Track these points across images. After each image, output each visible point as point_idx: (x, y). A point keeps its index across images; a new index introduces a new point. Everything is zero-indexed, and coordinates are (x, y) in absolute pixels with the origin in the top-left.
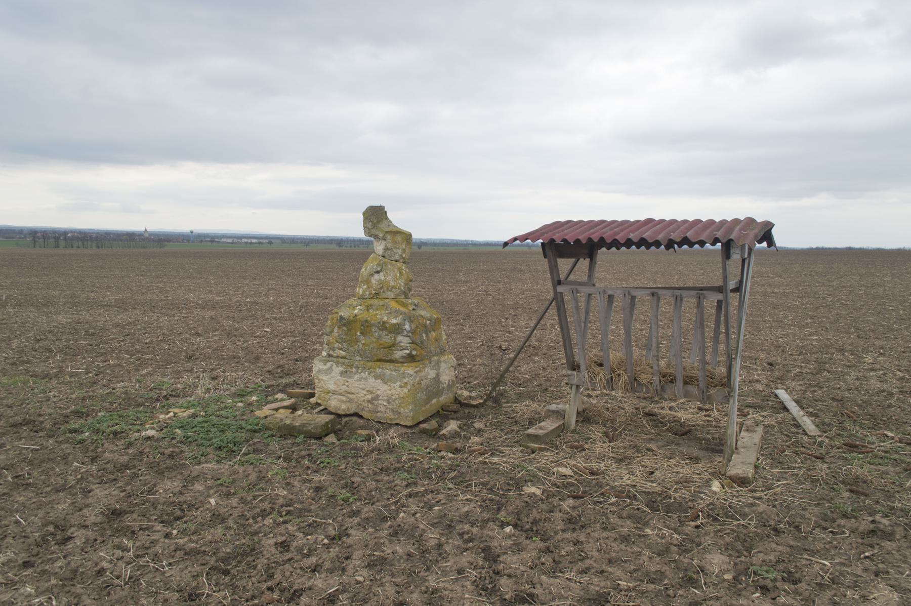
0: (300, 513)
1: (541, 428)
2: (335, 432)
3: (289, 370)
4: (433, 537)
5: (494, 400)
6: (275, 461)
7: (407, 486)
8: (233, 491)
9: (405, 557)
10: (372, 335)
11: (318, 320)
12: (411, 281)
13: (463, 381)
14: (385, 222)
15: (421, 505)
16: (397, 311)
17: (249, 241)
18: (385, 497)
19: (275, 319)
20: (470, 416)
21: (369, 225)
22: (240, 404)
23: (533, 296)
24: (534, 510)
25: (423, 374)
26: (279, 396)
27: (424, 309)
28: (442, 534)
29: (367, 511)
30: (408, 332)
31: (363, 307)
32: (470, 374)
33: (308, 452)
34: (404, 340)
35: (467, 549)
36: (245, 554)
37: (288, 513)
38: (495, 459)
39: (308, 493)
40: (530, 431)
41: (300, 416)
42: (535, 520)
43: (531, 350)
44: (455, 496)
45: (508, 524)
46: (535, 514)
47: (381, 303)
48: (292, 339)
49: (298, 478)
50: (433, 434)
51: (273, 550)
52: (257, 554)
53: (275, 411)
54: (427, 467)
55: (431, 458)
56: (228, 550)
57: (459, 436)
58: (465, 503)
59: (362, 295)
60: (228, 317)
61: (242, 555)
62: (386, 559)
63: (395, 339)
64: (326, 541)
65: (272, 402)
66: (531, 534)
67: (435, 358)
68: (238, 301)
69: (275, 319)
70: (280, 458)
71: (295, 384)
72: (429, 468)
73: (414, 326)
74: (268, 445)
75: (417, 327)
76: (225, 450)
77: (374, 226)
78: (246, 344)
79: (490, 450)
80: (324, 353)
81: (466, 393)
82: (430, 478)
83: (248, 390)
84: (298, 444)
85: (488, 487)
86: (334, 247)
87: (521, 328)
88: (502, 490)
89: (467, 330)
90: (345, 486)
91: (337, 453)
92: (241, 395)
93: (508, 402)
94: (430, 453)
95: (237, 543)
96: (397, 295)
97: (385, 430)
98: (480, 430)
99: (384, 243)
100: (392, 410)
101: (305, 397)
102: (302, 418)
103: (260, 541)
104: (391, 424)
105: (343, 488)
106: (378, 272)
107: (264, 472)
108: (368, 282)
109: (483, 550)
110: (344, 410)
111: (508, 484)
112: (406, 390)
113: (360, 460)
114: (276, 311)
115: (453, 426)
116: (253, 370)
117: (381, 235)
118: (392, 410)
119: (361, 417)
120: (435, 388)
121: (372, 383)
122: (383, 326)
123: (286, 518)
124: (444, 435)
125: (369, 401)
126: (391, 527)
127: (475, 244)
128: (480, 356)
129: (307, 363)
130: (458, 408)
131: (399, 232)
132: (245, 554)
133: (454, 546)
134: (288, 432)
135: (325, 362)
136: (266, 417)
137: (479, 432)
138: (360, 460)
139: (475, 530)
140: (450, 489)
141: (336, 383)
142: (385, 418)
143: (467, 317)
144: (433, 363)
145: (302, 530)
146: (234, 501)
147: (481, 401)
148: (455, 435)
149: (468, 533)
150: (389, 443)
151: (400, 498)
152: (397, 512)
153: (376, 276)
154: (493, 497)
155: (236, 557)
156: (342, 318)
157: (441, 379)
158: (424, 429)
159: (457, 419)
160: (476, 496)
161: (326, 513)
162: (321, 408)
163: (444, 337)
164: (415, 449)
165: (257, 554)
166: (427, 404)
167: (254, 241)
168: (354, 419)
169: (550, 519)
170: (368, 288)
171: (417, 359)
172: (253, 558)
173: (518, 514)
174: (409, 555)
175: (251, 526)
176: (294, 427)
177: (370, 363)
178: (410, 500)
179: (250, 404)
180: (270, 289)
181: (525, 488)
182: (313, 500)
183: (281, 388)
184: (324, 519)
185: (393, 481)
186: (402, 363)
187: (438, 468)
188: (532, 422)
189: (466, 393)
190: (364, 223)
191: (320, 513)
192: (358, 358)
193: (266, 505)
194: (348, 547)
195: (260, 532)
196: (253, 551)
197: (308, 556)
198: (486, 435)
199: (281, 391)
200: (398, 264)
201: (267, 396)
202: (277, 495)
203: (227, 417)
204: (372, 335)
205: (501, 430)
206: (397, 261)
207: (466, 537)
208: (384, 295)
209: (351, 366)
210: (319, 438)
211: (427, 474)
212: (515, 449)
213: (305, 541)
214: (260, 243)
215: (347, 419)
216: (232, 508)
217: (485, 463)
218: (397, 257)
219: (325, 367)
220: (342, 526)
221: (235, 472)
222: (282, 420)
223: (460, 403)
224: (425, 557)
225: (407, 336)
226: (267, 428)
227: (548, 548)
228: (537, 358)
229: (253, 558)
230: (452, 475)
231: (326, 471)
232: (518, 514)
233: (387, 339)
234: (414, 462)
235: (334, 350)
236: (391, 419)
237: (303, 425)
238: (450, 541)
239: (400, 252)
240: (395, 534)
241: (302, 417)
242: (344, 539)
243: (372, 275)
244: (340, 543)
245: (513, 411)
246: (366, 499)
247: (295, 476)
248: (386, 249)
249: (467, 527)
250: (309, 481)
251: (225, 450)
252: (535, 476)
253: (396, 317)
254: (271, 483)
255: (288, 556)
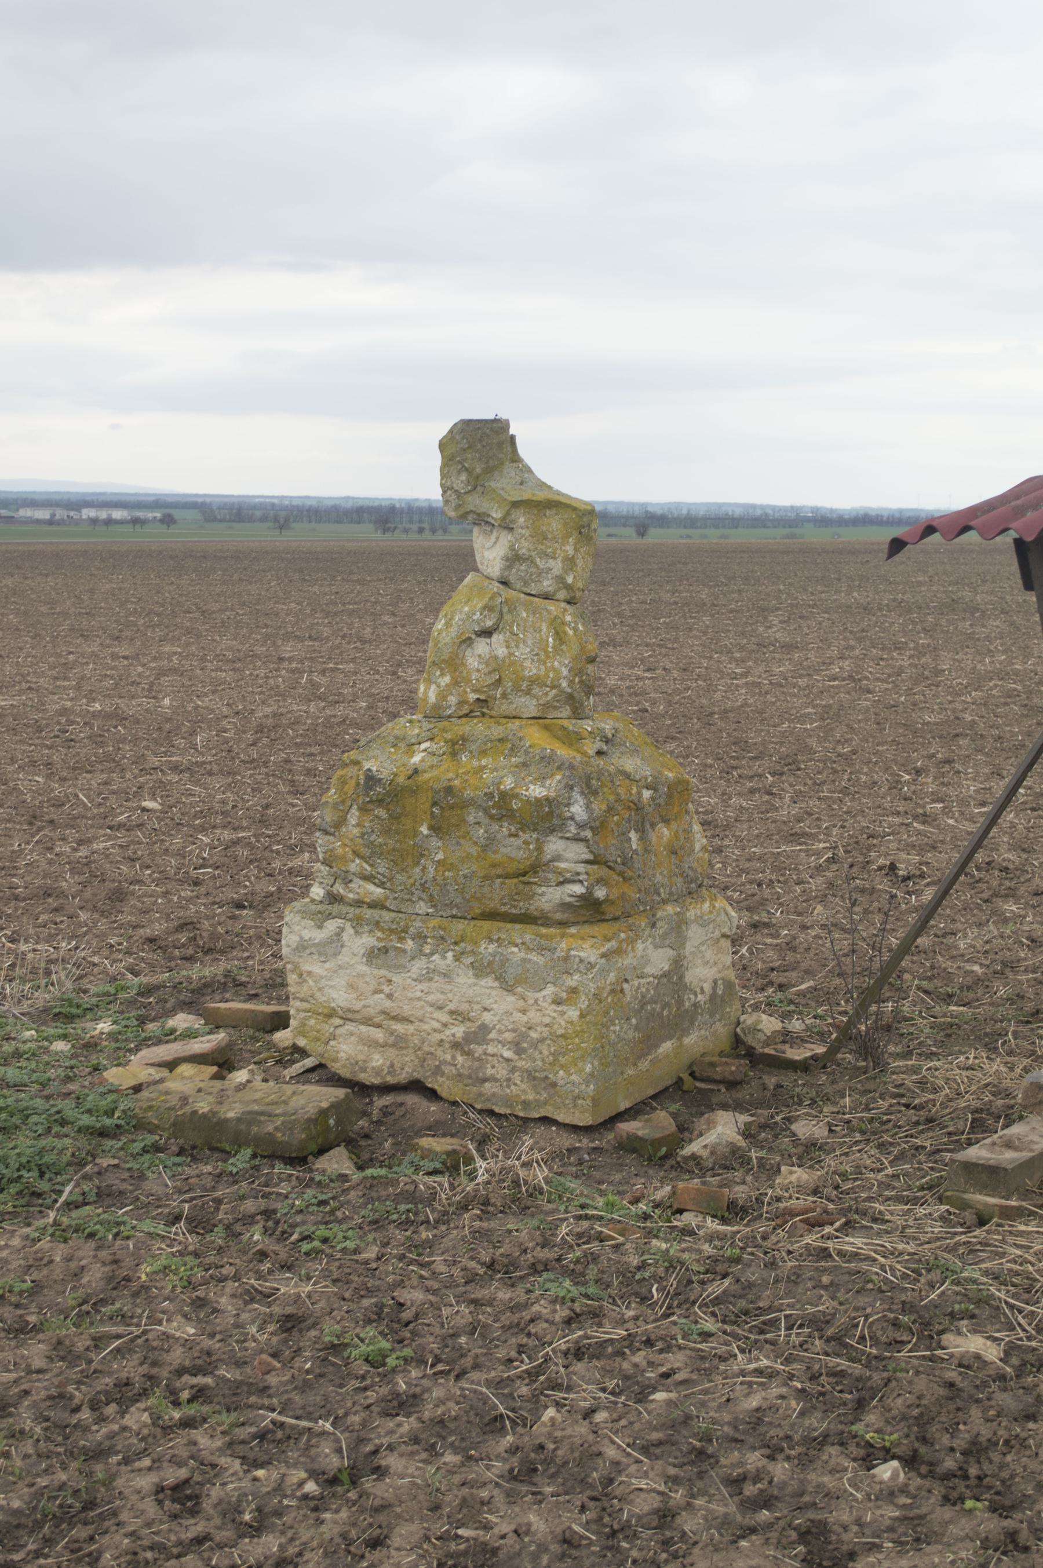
0: (236, 1397)
1: (1009, 1145)
2: (351, 1143)
3: (214, 936)
4: (644, 1487)
5: (862, 1046)
6: (161, 1229)
7: (568, 1322)
8: (32, 1319)
9: (555, 1548)
10: (466, 835)
11: (310, 772)
12: (592, 660)
13: (767, 981)
14: (509, 470)
15: (611, 1384)
16: (548, 759)
17: (103, 515)
18: (501, 1354)
19: (176, 768)
20: (779, 1098)
21: (460, 481)
22: (60, 1046)
23: (1010, 694)
24: (975, 1412)
25: (628, 961)
26: (181, 1021)
27: (635, 752)
28: (675, 1480)
29: (441, 1397)
30: (581, 826)
31: (439, 746)
32: (790, 957)
33: (263, 1204)
34: (567, 853)
35: (753, 1530)
36: (65, 1518)
37: (199, 1394)
38: (855, 1242)
39: (261, 1336)
40: (975, 1153)
41: (241, 1087)
42: (974, 1442)
43: (994, 878)
44: (722, 1359)
45: (888, 1454)
46: (976, 1424)
47: (497, 731)
48: (227, 835)
49: (231, 1286)
50: (662, 1156)
51: (150, 1507)
52: (102, 1517)
53: (166, 1071)
54: (635, 1261)
55: (651, 1234)
56: (16, 1504)
57: (745, 1161)
58: (753, 1383)
59: (436, 707)
60: (33, 763)
61: (58, 1521)
62: (495, 1551)
63: (540, 849)
64: (311, 1487)
65: (159, 1042)
66: (961, 1486)
67: (670, 909)
68: (64, 711)
69: (176, 768)
70: (177, 1218)
71: (230, 984)
72: (642, 1266)
73: (599, 807)
74: (142, 1177)
75: (610, 809)
76: (13, 1189)
77: (476, 484)
78: (83, 852)
79: (843, 1212)
80: (317, 892)
81: (769, 1024)
82: (644, 1299)
83: (87, 1000)
84: (234, 1178)
85: (830, 1332)
86: (367, 534)
87: (964, 802)
88: (875, 1341)
89: (786, 810)
90: (376, 1316)
91: (355, 1209)
92: (65, 1015)
93: (907, 1055)
94: (646, 1217)
95: (42, 1481)
96: (547, 706)
97: (506, 1137)
98: (812, 1145)
99: (506, 538)
100: (530, 1076)
101: (259, 1031)
102: (246, 1095)
103: (112, 1477)
104: (526, 1120)
105: (369, 1321)
106: (487, 633)
107: (128, 1262)
108: (453, 664)
109: (804, 1536)
110: (378, 1072)
111: (896, 1324)
112: (573, 1014)
113: (425, 1234)
114: (180, 742)
115: (723, 1129)
116: (102, 936)
117: (497, 514)
118: (530, 1076)
119: (432, 1094)
120: (667, 1008)
121: (468, 987)
122: (502, 807)
123: (191, 1411)
124: (694, 1157)
125: (456, 1045)
126: (514, 1450)
127: (823, 520)
128: (823, 899)
129: (270, 915)
130: (741, 1074)
131: (554, 504)
132: (65, 1518)
133: (710, 1521)
134: (203, 1139)
135: (320, 919)
136: (137, 1089)
137: (809, 1152)
138: (425, 1234)
139: (780, 1470)
140: (706, 1336)
141: (359, 988)
142: (508, 1101)
143: (790, 765)
144: (662, 927)
145: (240, 1449)
146: (36, 1352)
147: (821, 1050)
148: (731, 1159)
149: (757, 1479)
150: (516, 1183)
151: (547, 1359)
152: (536, 1404)
153: (481, 647)
154: (843, 1363)
155: (38, 1525)
156: (371, 779)
157: (689, 977)
158: (631, 1138)
159: (738, 1107)
160: (788, 1361)
161: (314, 1398)
162: (309, 1062)
163: (700, 841)
164: (601, 1202)
165: (102, 1517)
166: (641, 1056)
167: (117, 514)
168: (411, 1099)
169: (1023, 1443)
170: (456, 683)
171: (611, 911)
172: (89, 1530)
173: (923, 1421)
174: (568, 1541)
175: (86, 1429)
176: (222, 1124)
177: (460, 926)
178: (579, 1367)
179: (92, 1046)
180: (162, 673)
181: (948, 1338)
182: (274, 1355)
183: (185, 996)
184: (309, 1417)
185: (526, 1305)
186: (563, 924)
187: (670, 1267)
188: (981, 1124)
189: (769, 1024)
190: (443, 476)
191: (297, 1398)
192: (422, 908)
193: (131, 1368)
194: (377, 1510)
195: (110, 1451)
196: (89, 1508)
197: (256, 1530)
198: (831, 1162)
199: (187, 1006)
200: (551, 606)
201: (142, 1021)
202: (167, 1336)
203: (19, 1086)
204: (466, 835)
205: (881, 1146)
206: (546, 597)
207: (750, 1490)
208: (505, 708)
209: (401, 933)
210: (299, 1160)
211: (634, 1285)
212: (921, 1211)
213: (246, 1484)
214: (135, 521)
215: (387, 1100)
216: (29, 1372)
217: (824, 1254)
218: (547, 584)
219: (319, 936)
220: (362, 1441)
221: (42, 1262)
222: (184, 1100)
223: (751, 1054)
224: (617, 1549)
225: (577, 839)
226: (140, 1126)
227: (1012, 1536)
228: (1011, 907)
229: (89, 1530)
230: (717, 1288)
231: (316, 1267)
232: (923, 1421)
233: (514, 848)
234: (594, 1246)
235: (347, 882)
236: (526, 1104)
237: (250, 1118)
238: (699, 1502)
239: (557, 566)
240: (525, 1473)
241: (250, 1092)
242: (368, 1483)
243: (468, 642)
244: (352, 1495)
245: (922, 1083)
246: (438, 1360)
247: (223, 1279)
248: (513, 559)
249: (754, 1459)
250: (266, 1296)
251: (13, 1189)
252: (984, 1301)
253: (542, 779)
254: (150, 1300)
255: (195, 1528)
